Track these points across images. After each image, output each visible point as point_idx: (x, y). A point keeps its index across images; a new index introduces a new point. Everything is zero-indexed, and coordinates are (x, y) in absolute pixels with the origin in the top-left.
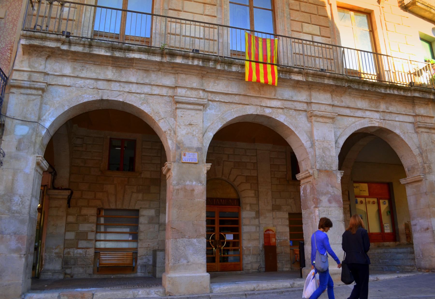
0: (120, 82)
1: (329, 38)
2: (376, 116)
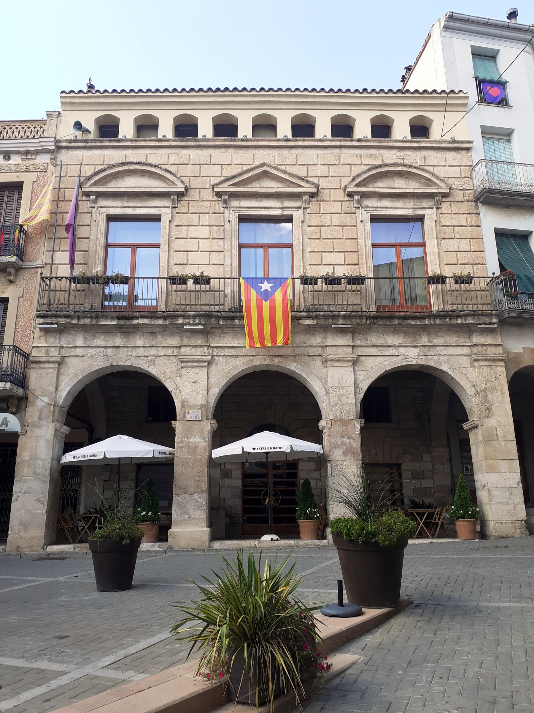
0: (127, 347)
2: (416, 351)
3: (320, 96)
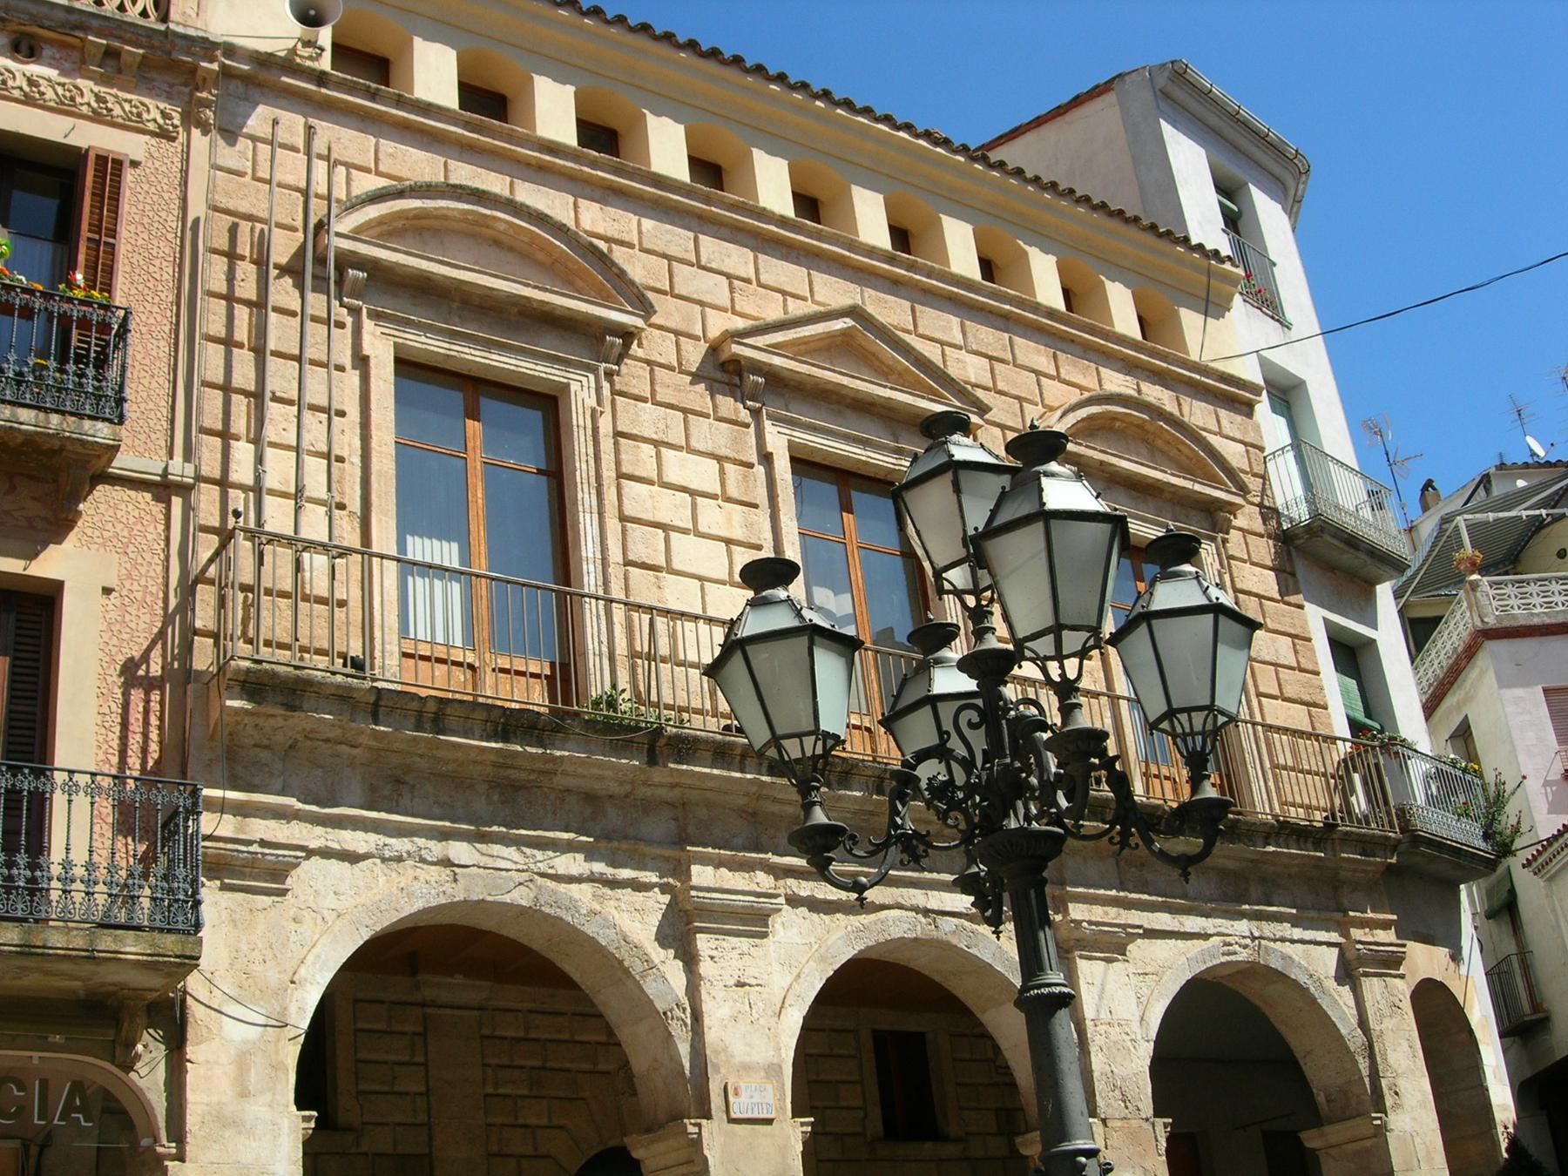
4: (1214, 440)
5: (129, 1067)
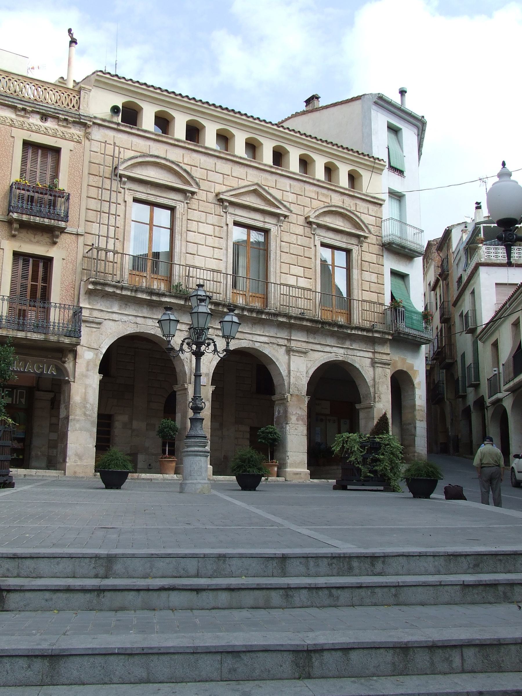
1: (311, 279)
2: (342, 351)
3: (230, 115)
4: (355, 212)
5: (64, 362)
